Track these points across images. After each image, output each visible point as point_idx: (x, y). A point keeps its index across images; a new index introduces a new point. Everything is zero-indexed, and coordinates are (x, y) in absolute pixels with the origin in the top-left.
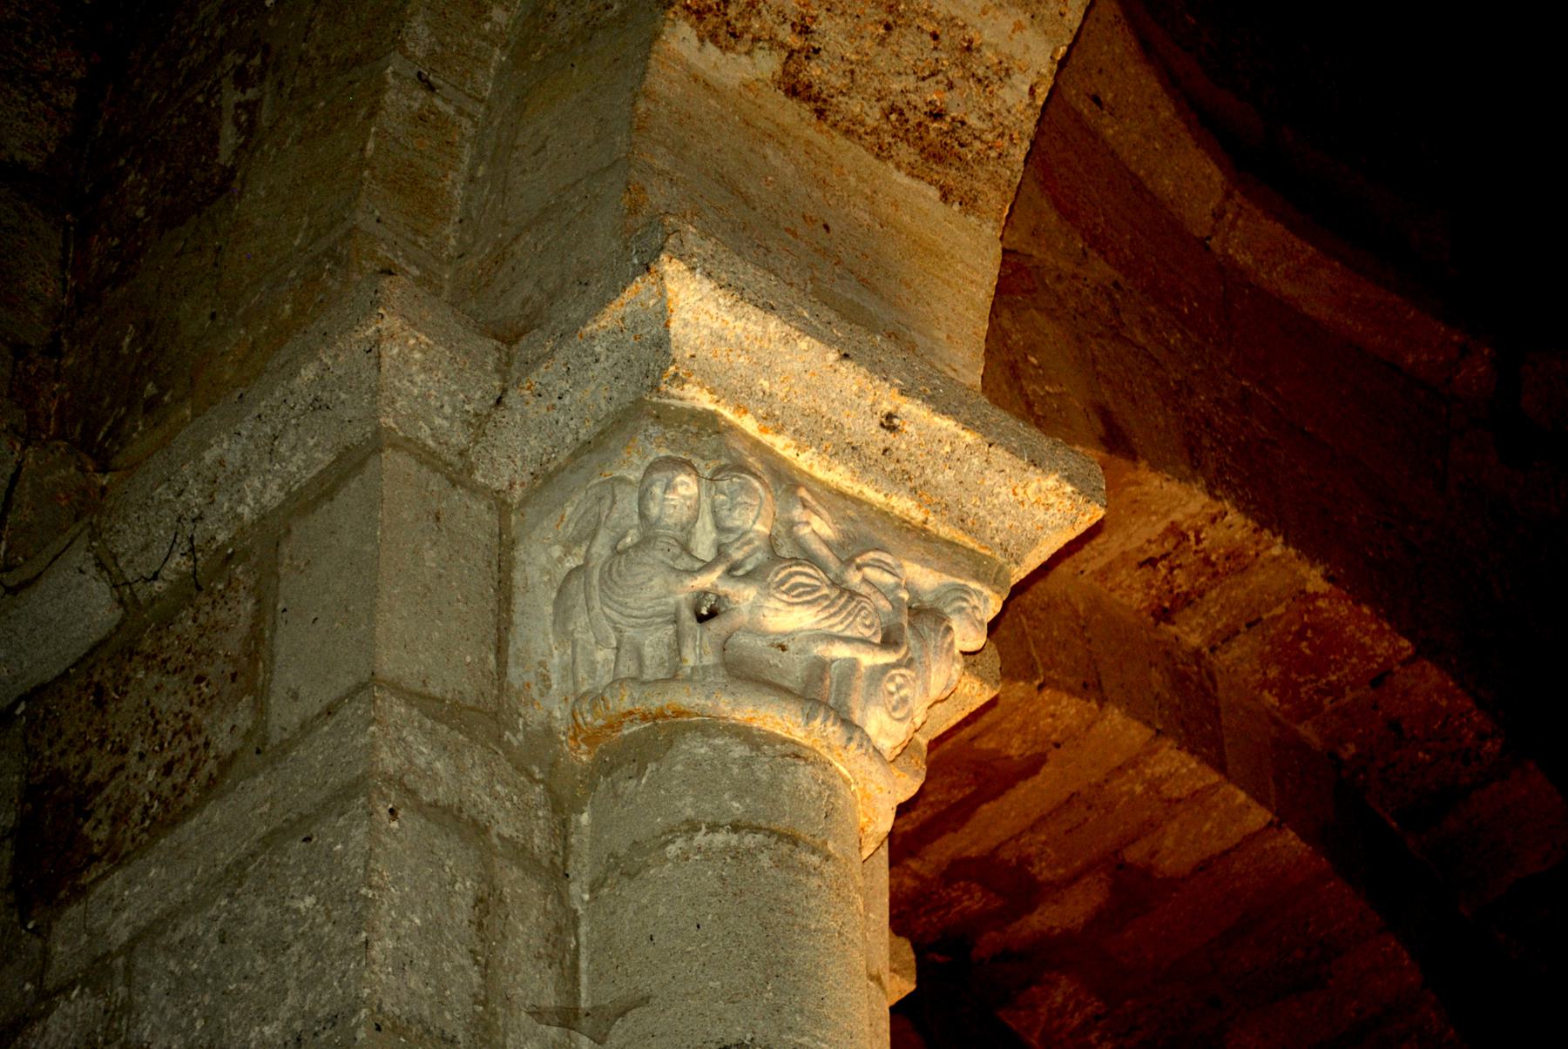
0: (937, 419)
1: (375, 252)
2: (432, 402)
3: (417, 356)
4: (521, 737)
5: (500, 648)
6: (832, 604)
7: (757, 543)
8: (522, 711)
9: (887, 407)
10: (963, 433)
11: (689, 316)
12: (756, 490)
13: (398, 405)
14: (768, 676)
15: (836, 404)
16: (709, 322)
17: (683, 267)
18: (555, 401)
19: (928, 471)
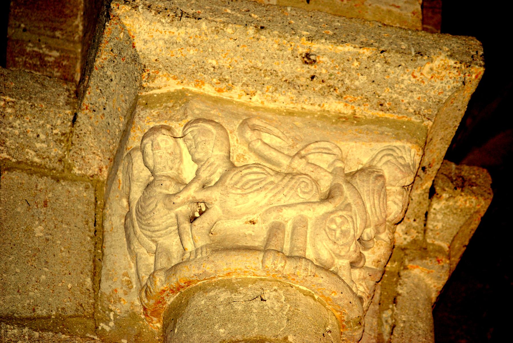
0: (340, 48)
1: (25, 50)
2: (30, 134)
3: (9, 110)
4: (112, 324)
5: (96, 275)
6: (277, 186)
7: (217, 163)
8: (112, 307)
9: (302, 50)
10: (361, 51)
11: (146, 37)
12: (209, 131)
13: (8, 144)
14: (242, 243)
15: (267, 60)
16: (161, 36)
17: (128, 8)
18: (103, 111)
19: (347, 81)
